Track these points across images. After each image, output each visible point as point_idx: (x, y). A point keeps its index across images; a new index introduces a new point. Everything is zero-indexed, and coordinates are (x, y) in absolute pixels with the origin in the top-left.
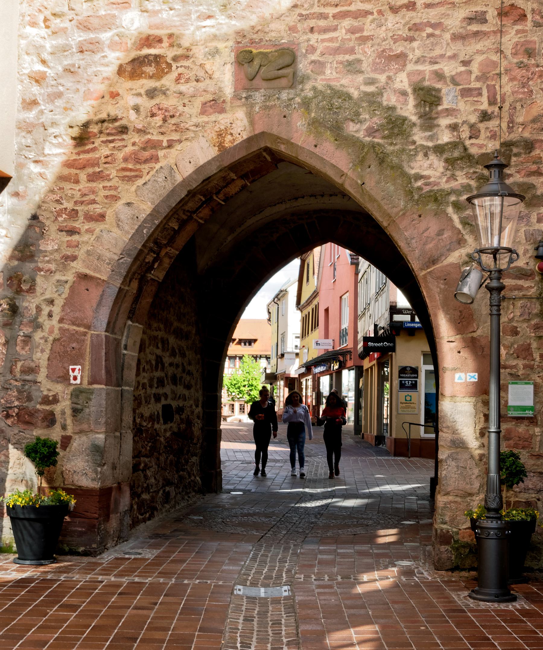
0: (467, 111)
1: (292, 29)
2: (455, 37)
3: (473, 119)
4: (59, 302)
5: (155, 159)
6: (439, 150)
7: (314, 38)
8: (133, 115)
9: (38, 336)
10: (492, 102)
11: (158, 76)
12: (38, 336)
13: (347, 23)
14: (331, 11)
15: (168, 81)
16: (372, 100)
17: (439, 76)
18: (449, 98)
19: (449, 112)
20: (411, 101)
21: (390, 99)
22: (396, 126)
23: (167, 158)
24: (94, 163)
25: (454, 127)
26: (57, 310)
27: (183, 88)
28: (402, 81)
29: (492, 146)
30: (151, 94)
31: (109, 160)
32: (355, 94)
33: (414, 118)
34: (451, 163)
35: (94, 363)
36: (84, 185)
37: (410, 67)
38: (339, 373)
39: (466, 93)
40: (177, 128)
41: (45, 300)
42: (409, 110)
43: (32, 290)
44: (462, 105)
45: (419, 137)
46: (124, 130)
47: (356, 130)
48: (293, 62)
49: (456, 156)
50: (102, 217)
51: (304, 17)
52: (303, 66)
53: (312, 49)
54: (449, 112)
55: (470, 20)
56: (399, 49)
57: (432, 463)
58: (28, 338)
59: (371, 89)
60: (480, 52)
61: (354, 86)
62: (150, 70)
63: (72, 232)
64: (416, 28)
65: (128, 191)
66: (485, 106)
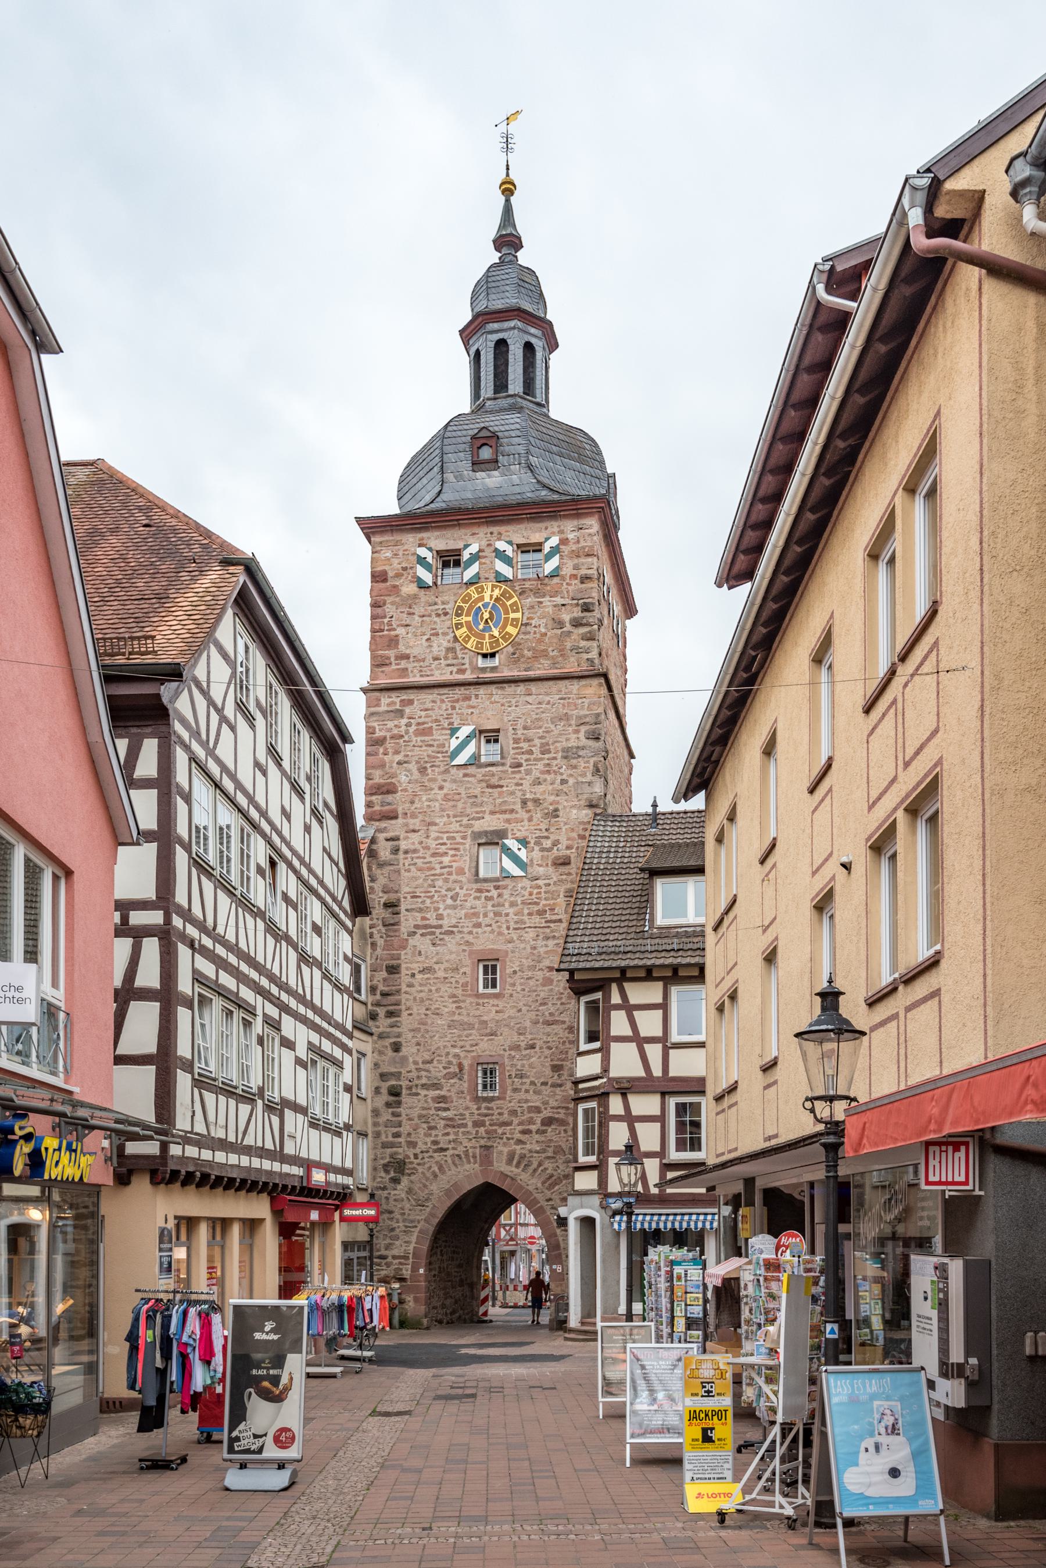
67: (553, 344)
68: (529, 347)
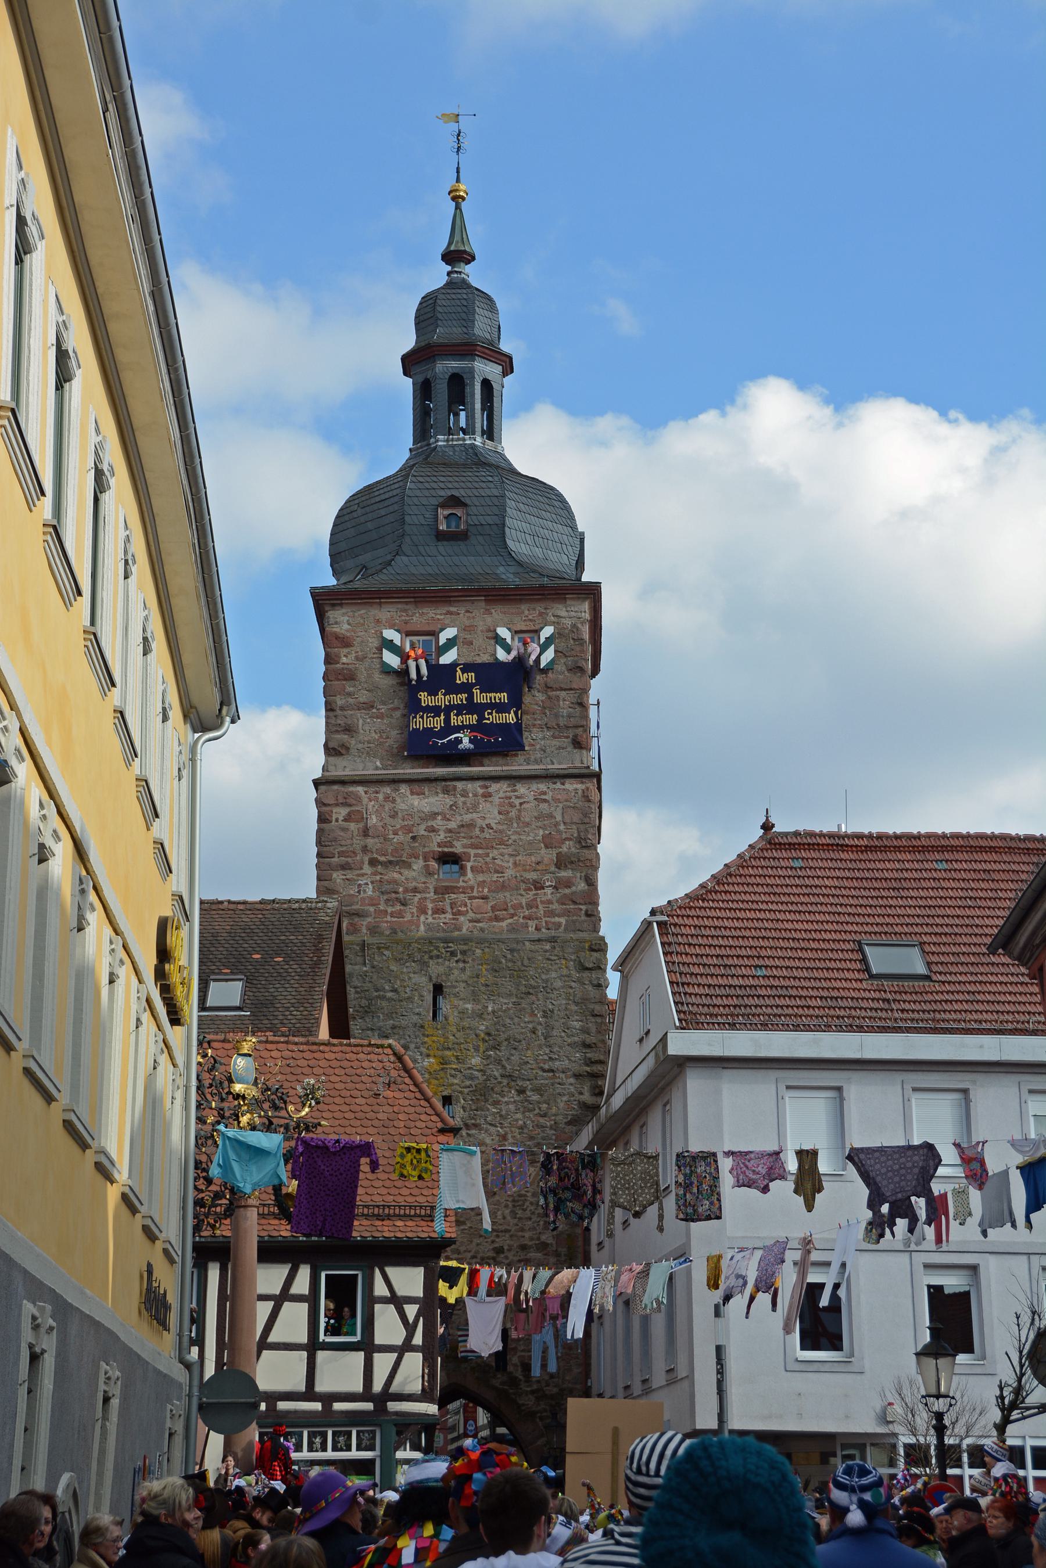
6: (533, 1392)
29: (555, 1390)
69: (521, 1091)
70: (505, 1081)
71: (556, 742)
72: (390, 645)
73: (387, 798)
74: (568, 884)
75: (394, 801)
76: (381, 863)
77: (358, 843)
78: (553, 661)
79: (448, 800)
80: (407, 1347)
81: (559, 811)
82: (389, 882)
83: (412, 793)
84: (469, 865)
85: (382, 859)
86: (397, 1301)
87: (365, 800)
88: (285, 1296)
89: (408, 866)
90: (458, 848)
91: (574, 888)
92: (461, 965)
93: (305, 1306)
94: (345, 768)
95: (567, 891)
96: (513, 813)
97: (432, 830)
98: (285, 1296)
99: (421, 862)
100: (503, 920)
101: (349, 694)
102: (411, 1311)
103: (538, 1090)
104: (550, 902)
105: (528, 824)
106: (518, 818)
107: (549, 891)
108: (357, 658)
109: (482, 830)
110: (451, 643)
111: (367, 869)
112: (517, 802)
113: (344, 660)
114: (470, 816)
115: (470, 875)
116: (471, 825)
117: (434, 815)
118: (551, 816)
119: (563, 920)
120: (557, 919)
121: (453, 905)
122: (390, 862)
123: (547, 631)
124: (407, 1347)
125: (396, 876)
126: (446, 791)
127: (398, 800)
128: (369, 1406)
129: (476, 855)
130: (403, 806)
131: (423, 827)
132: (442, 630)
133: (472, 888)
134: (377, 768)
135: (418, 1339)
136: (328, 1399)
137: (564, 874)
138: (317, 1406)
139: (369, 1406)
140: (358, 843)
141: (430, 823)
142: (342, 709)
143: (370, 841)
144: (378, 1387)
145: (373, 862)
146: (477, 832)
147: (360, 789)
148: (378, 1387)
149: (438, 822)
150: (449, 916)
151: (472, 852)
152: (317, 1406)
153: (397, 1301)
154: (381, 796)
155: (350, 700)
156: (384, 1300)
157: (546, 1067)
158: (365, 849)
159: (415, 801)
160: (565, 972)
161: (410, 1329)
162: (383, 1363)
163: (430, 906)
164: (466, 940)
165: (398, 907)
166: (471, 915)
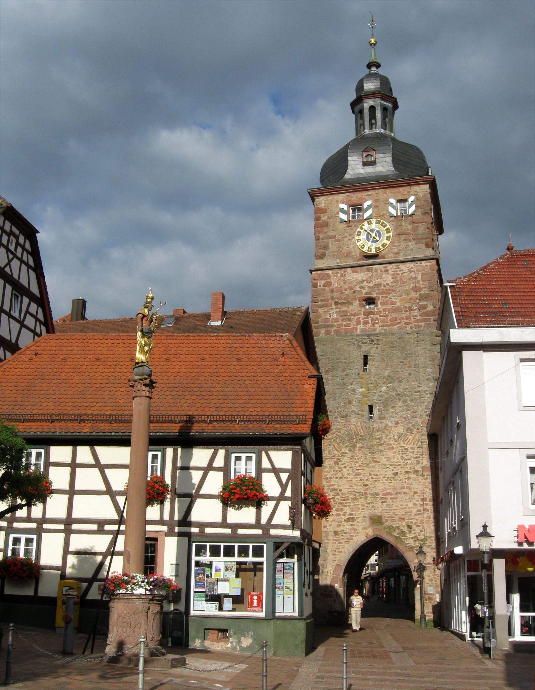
0: (417, 530)
1: (381, 512)
2: (415, 515)
3: (419, 532)
4: (332, 570)
5: (352, 539)
6: (412, 538)
7: (386, 514)
8: (348, 530)
9: (328, 577)
10: (423, 528)
11: (353, 522)
12: (328, 577)
13: (393, 511)
14: (389, 509)
15: (355, 523)
16: (398, 527)
17: (412, 523)
18: (414, 527)
19: (414, 530)
20: (406, 528)
21: (401, 528)
22: (403, 533)
23: (355, 539)
24: (339, 540)
25: (415, 533)
26: (332, 572)
27: (358, 524)
28: (404, 523)
29: (423, 537)
30: (351, 525)
31: (343, 539)
32: (395, 526)
33: (407, 532)
34: (415, 541)
35: (340, 584)
36: (337, 544)
37: (406, 521)
38: (398, 577)
39: (417, 526)
40: (357, 533)
41: (75, 655)
42: (406, 529)
43: (326, 568)
44: (416, 529)
45: (408, 535)
46: (346, 533)
47: (395, 534)
48: (381, 519)
49: (415, 539)
50: (341, 552)
51: (383, 510)
52: (384, 520)
53: (385, 516)
54: (414, 530)
55: (418, 511)
56: (403, 517)
57: (467, 356)
58: (326, 578)
59: (398, 525)
60: (419, 518)
61: (395, 525)
62: (351, 520)
63: (335, 555)
64: (407, 513)
65: (347, 546)
66: (421, 529)
67: (396, 106)
68: (385, 109)
69: (405, 402)
70: (397, 397)
71: (418, 246)
72: (342, 211)
73: (342, 275)
74: (425, 307)
75: (345, 276)
76: (340, 303)
77: (329, 295)
78: (415, 211)
79: (369, 274)
80: (282, 497)
81: (420, 275)
82: (343, 311)
83: (353, 272)
84: (379, 302)
85: (340, 301)
86: (276, 471)
87: (332, 277)
88: (210, 468)
89: (351, 304)
90: (374, 295)
91: (427, 309)
92: (376, 346)
93: (221, 474)
94: (320, 264)
95: (424, 311)
96: (398, 278)
97: (362, 287)
98: (210, 468)
99: (357, 302)
100: (395, 325)
101: (326, 233)
102: (284, 477)
103: (412, 400)
104: (416, 316)
105: (404, 282)
106: (401, 279)
107: (416, 311)
108: (328, 218)
109: (384, 286)
110: (369, 207)
111: (333, 306)
112: (400, 273)
113: (323, 219)
114: (379, 280)
115: (380, 306)
116: (379, 285)
117: (362, 281)
118: (416, 278)
119: (423, 324)
120: (420, 324)
121: (372, 320)
122: (344, 303)
123: (411, 199)
124: (282, 497)
125: (347, 309)
126: (368, 270)
127: (347, 276)
128: (259, 532)
129: (382, 297)
130: (349, 278)
131: (358, 287)
132: (365, 202)
133: (381, 312)
134: (338, 263)
135: (288, 493)
136: (235, 527)
137: (422, 303)
138: (228, 531)
139: (259, 532)
140: (329, 295)
141: (361, 285)
142: (322, 239)
143: (335, 294)
144: (264, 521)
145: (336, 303)
146: (382, 287)
147: (330, 272)
148: (264, 520)
149: (365, 283)
150: (370, 324)
151: (380, 296)
152: (228, 531)
153: (276, 471)
154: (339, 274)
155: (325, 235)
156: (267, 470)
157: (416, 390)
158: (332, 298)
159: (355, 275)
160: (424, 346)
161: (284, 487)
162: (267, 509)
163: (362, 321)
164: (378, 335)
165: (348, 322)
166: (380, 324)
